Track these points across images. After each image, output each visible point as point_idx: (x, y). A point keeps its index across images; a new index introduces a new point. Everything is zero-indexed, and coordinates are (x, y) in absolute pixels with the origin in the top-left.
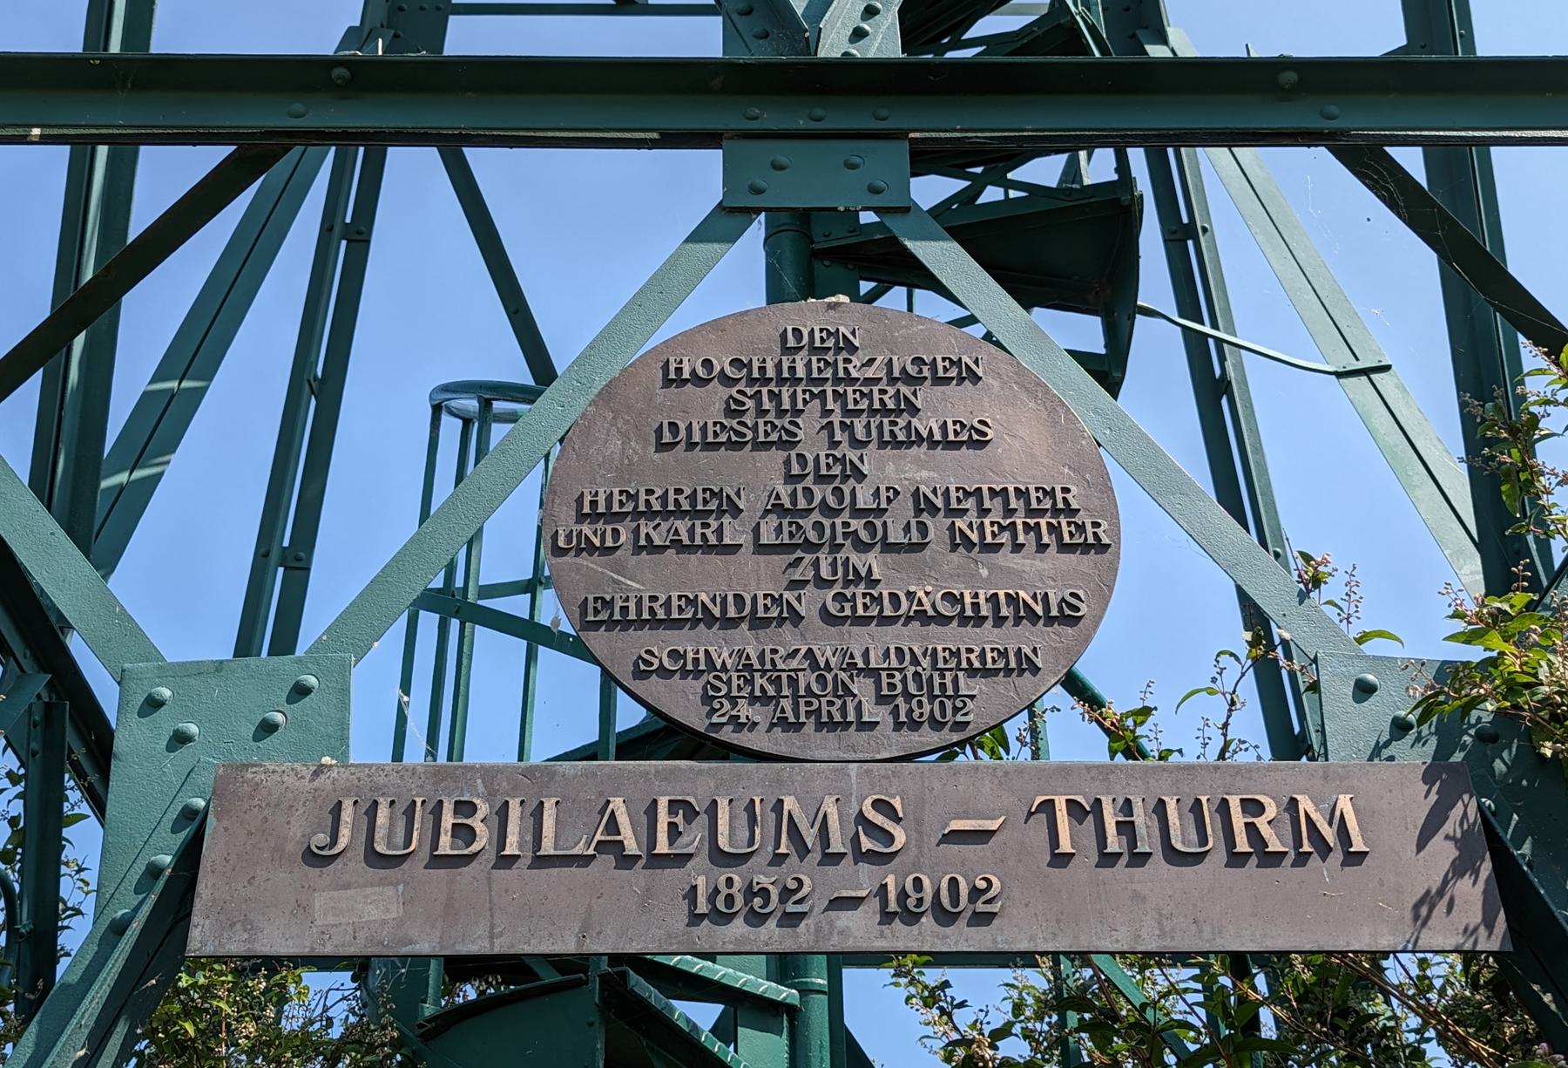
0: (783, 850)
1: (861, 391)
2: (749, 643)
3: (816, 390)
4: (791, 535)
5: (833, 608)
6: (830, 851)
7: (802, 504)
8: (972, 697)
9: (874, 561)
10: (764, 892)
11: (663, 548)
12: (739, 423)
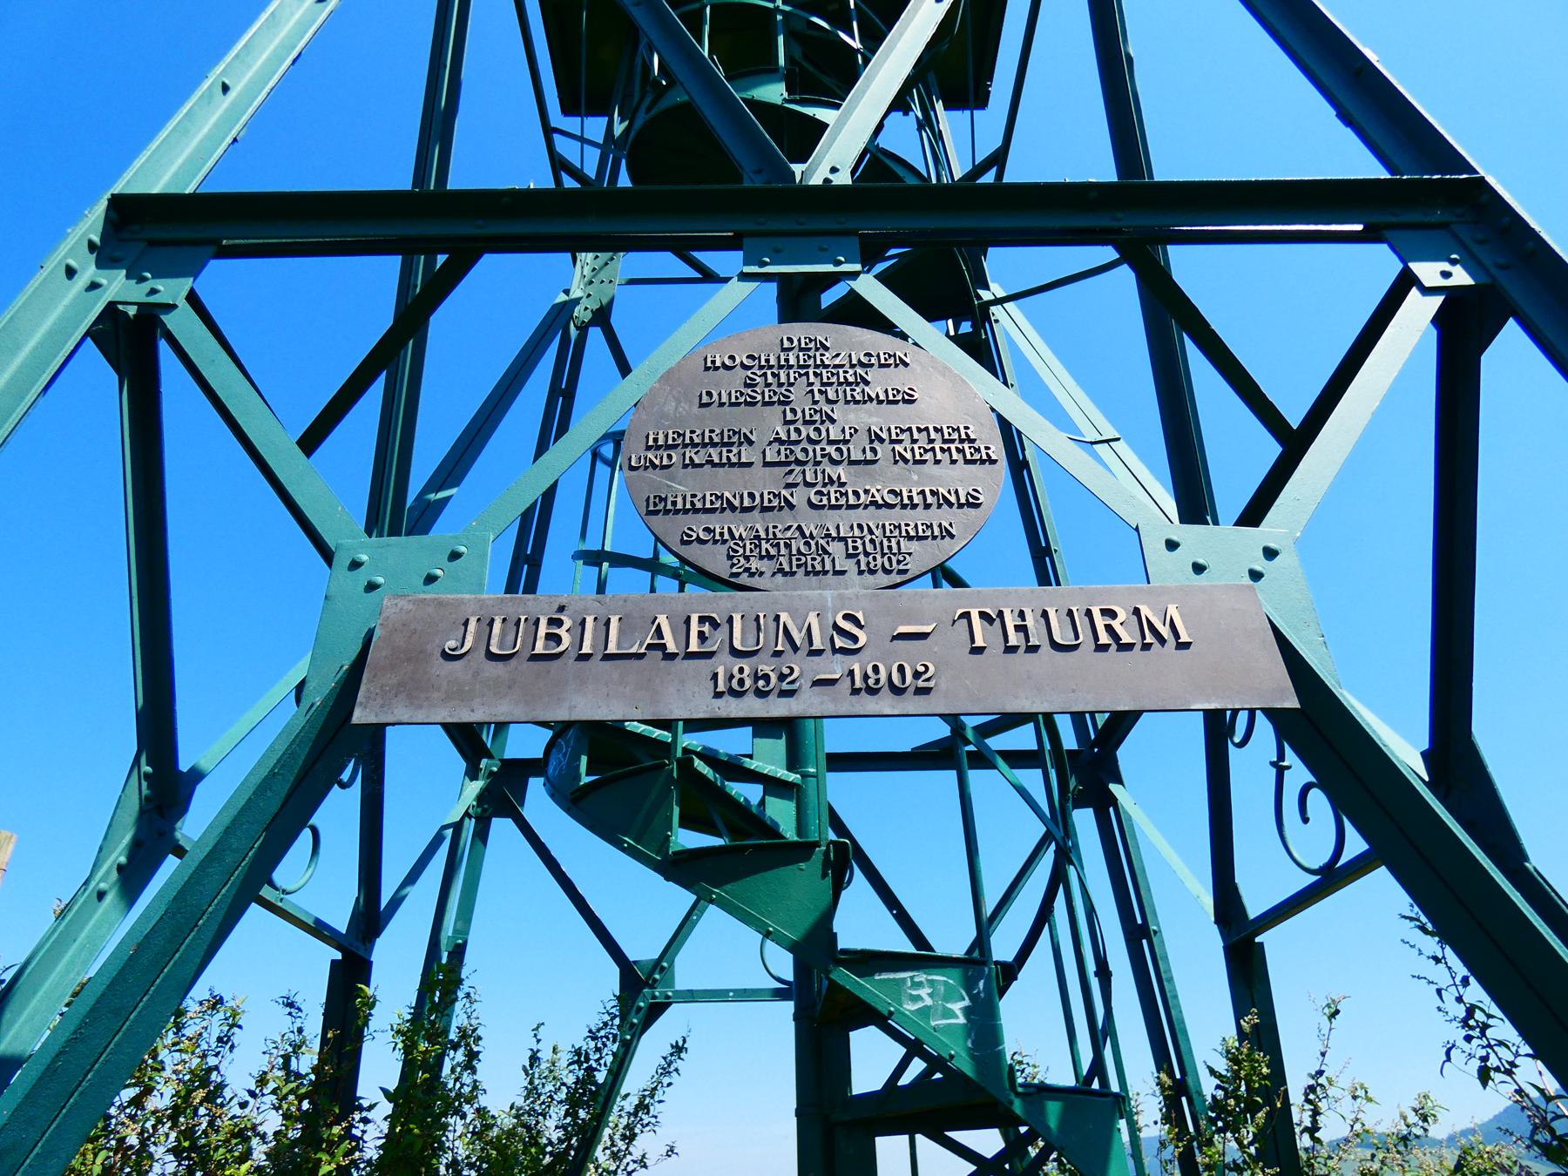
0: (779, 648)
1: (831, 372)
2: (759, 522)
3: (802, 372)
4: (787, 456)
5: (815, 500)
6: (813, 648)
7: (794, 436)
8: (910, 554)
9: (841, 471)
10: (766, 677)
11: (701, 465)
12: (752, 391)
